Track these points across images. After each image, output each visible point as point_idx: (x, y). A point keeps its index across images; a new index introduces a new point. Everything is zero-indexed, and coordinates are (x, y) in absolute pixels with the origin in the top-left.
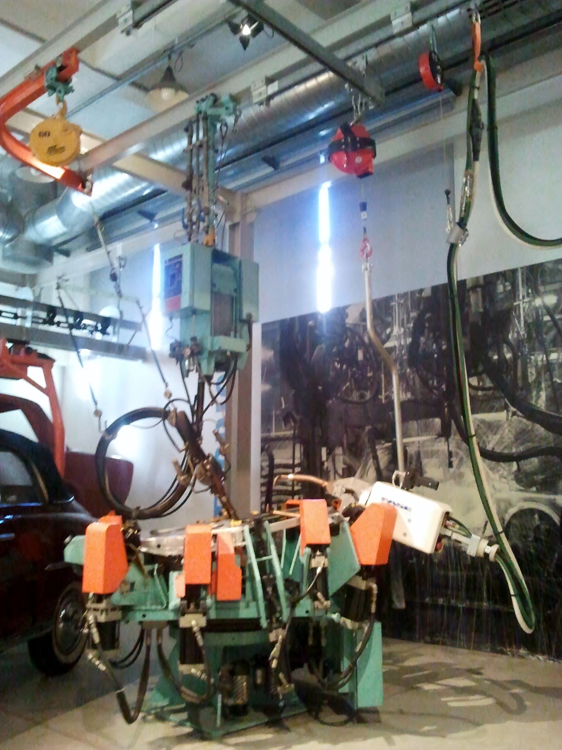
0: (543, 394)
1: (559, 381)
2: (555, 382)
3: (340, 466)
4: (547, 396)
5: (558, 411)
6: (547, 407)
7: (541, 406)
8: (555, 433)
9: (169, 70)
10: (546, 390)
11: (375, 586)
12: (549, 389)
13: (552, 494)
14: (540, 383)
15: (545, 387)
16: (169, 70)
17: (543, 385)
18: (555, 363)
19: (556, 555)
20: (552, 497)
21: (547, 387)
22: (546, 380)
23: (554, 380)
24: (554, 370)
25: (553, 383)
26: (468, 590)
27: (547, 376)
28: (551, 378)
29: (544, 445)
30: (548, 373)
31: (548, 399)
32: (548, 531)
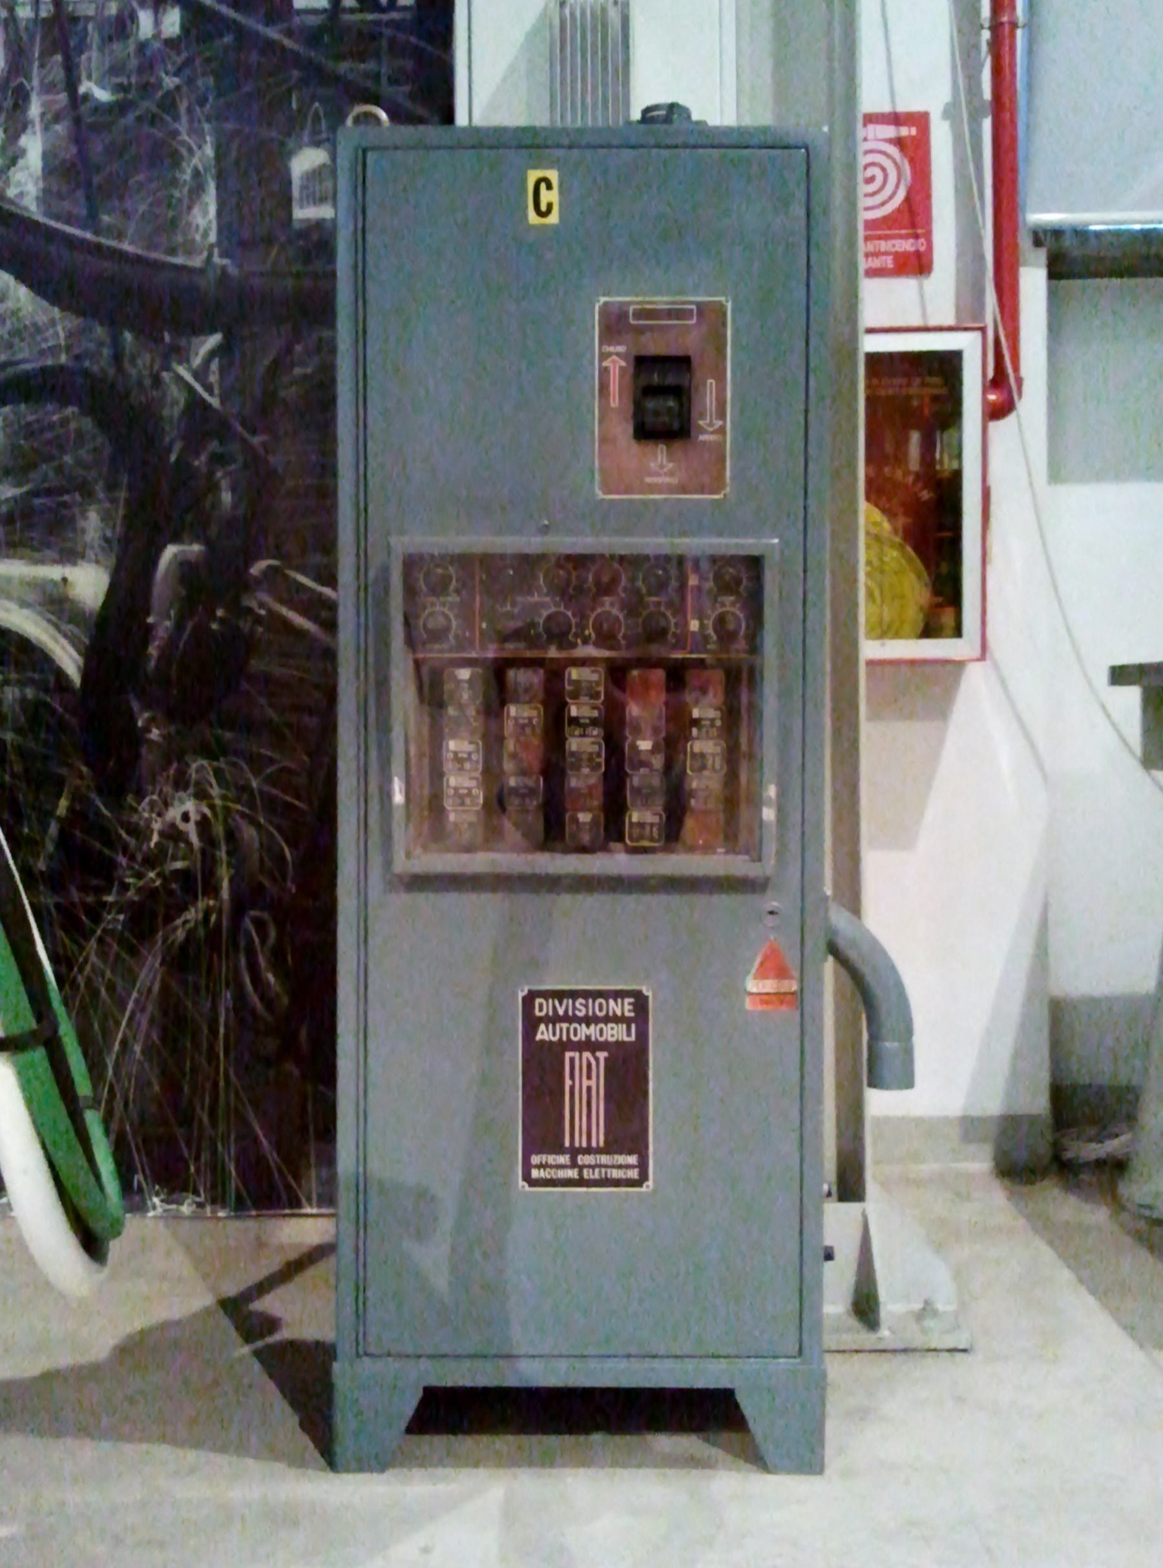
0: (33, 146)
1: (103, 95)
2: (87, 97)
3: (648, 828)
4: (45, 155)
5: (91, 221)
6: (47, 197)
7: (21, 195)
8: (80, 313)
9: (258, 1238)
10: (46, 128)
11: (253, 913)
12: (60, 128)
13: (55, 562)
14: (21, 98)
15: (43, 115)
16: (258, 1238)
17: (35, 110)
18: (88, 19)
19: (63, 803)
20: (54, 572)
21: (51, 119)
22: (48, 88)
23: (82, 89)
24: (82, 48)
25: (77, 101)
26: (834, 400)
27: (57, 73)
28: (72, 85)
29: (27, 357)
30: (59, 58)
31: (53, 168)
32: (35, 713)
